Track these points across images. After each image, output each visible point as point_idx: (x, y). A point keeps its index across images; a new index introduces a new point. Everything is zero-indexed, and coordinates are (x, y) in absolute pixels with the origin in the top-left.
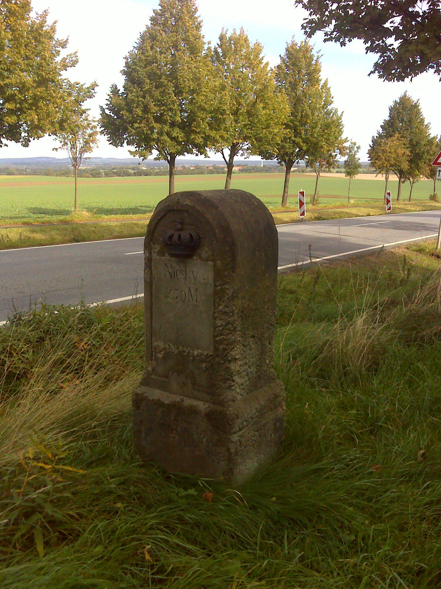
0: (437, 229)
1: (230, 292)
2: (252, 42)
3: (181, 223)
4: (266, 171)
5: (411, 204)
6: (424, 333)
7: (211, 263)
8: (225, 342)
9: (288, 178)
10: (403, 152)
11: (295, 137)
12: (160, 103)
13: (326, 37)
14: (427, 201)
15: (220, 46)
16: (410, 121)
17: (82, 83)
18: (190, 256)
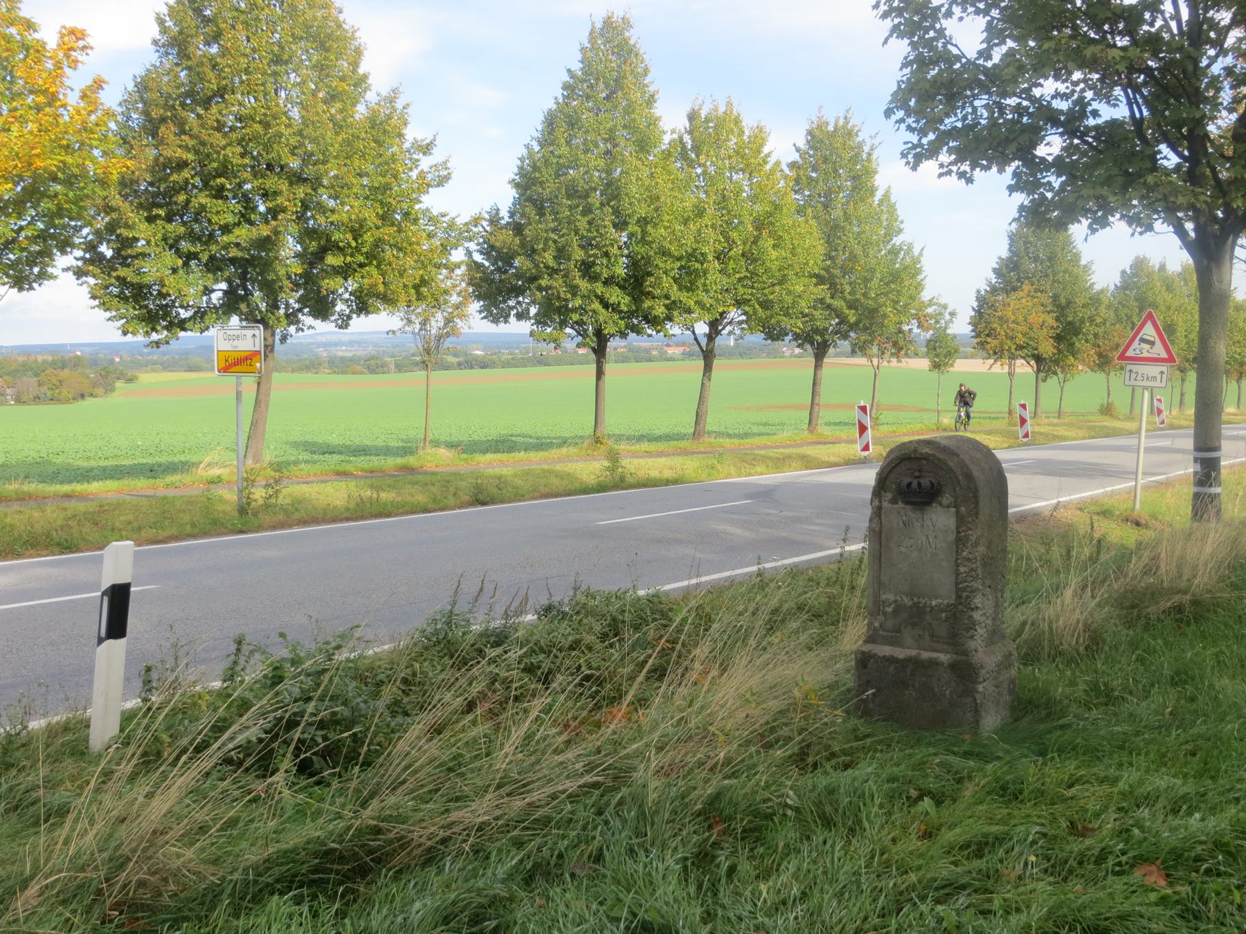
0: (1133, 473)
1: (973, 538)
2: (748, 123)
3: (919, 471)
4: (742, 355)
5: (1065, 424)
6: (1149, 610)
7: (953, 510)
8: (969, 589)
9: (819, 376)
10: (1041, 320)
11: (832, 297)
12: (587, 245)
13: (941, 171)
14: (1093, 418)
15: (690, 132)
16: (1050, 259)
17: (452, 215)
18: (929, 503)
